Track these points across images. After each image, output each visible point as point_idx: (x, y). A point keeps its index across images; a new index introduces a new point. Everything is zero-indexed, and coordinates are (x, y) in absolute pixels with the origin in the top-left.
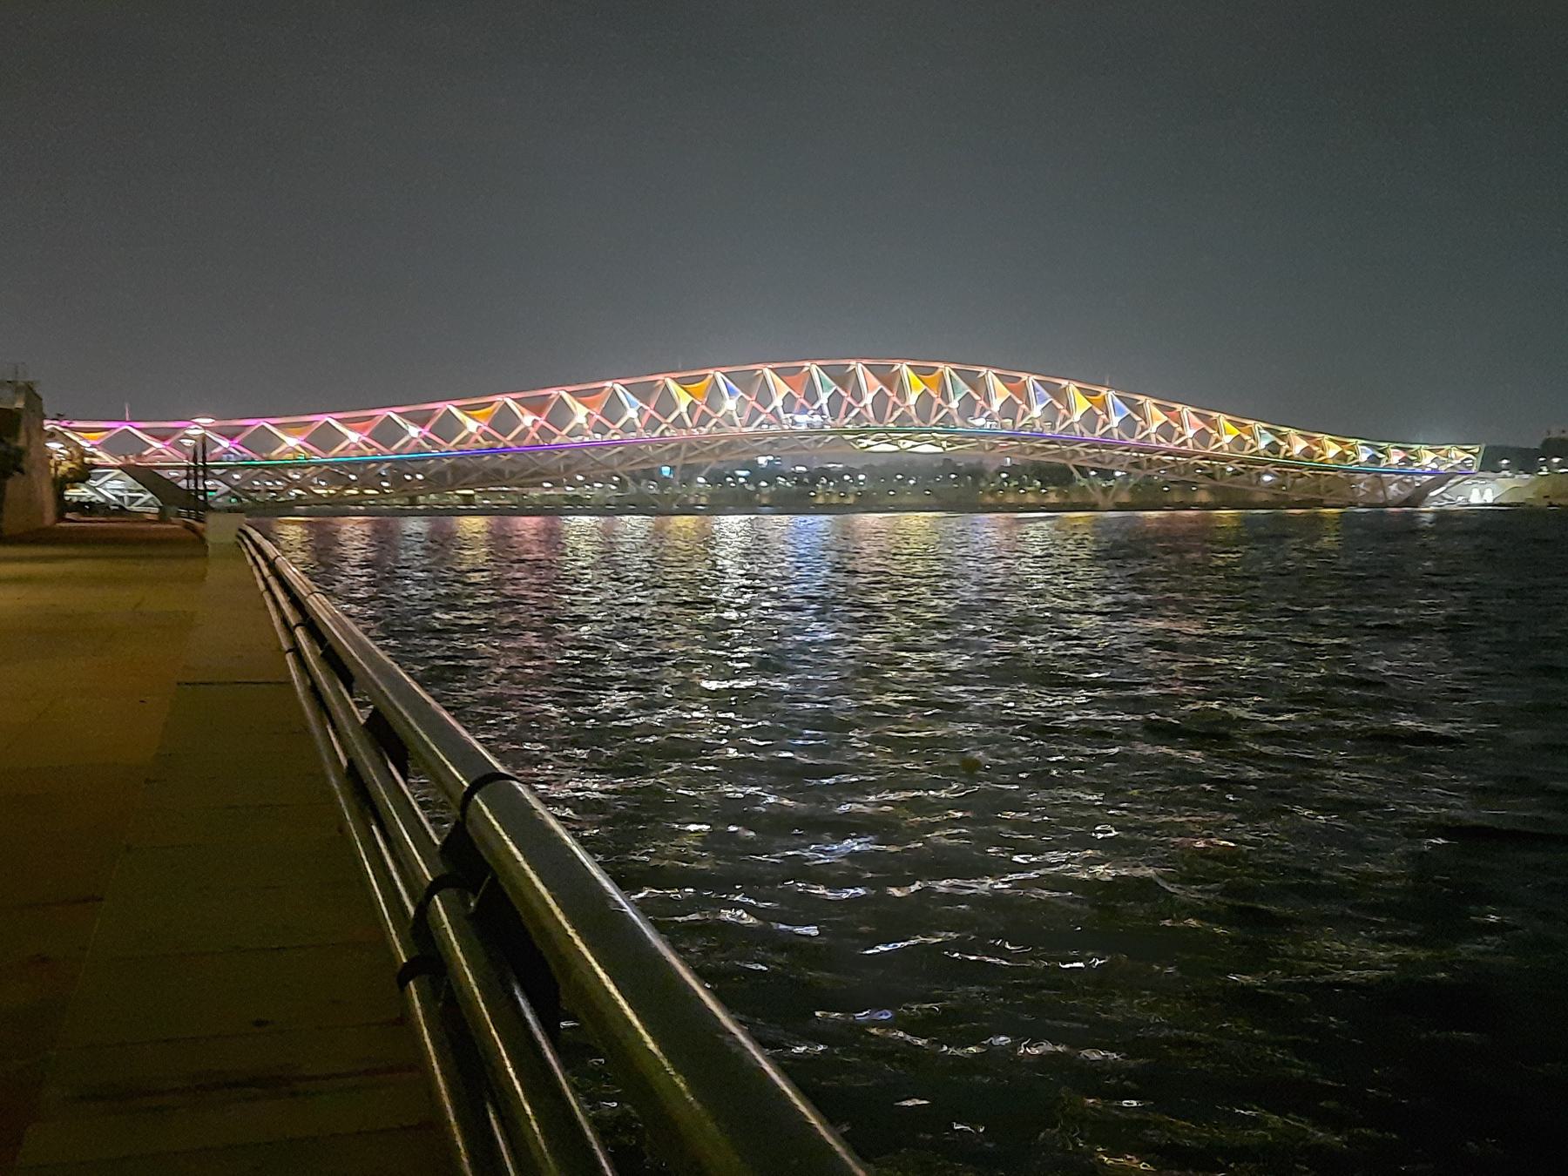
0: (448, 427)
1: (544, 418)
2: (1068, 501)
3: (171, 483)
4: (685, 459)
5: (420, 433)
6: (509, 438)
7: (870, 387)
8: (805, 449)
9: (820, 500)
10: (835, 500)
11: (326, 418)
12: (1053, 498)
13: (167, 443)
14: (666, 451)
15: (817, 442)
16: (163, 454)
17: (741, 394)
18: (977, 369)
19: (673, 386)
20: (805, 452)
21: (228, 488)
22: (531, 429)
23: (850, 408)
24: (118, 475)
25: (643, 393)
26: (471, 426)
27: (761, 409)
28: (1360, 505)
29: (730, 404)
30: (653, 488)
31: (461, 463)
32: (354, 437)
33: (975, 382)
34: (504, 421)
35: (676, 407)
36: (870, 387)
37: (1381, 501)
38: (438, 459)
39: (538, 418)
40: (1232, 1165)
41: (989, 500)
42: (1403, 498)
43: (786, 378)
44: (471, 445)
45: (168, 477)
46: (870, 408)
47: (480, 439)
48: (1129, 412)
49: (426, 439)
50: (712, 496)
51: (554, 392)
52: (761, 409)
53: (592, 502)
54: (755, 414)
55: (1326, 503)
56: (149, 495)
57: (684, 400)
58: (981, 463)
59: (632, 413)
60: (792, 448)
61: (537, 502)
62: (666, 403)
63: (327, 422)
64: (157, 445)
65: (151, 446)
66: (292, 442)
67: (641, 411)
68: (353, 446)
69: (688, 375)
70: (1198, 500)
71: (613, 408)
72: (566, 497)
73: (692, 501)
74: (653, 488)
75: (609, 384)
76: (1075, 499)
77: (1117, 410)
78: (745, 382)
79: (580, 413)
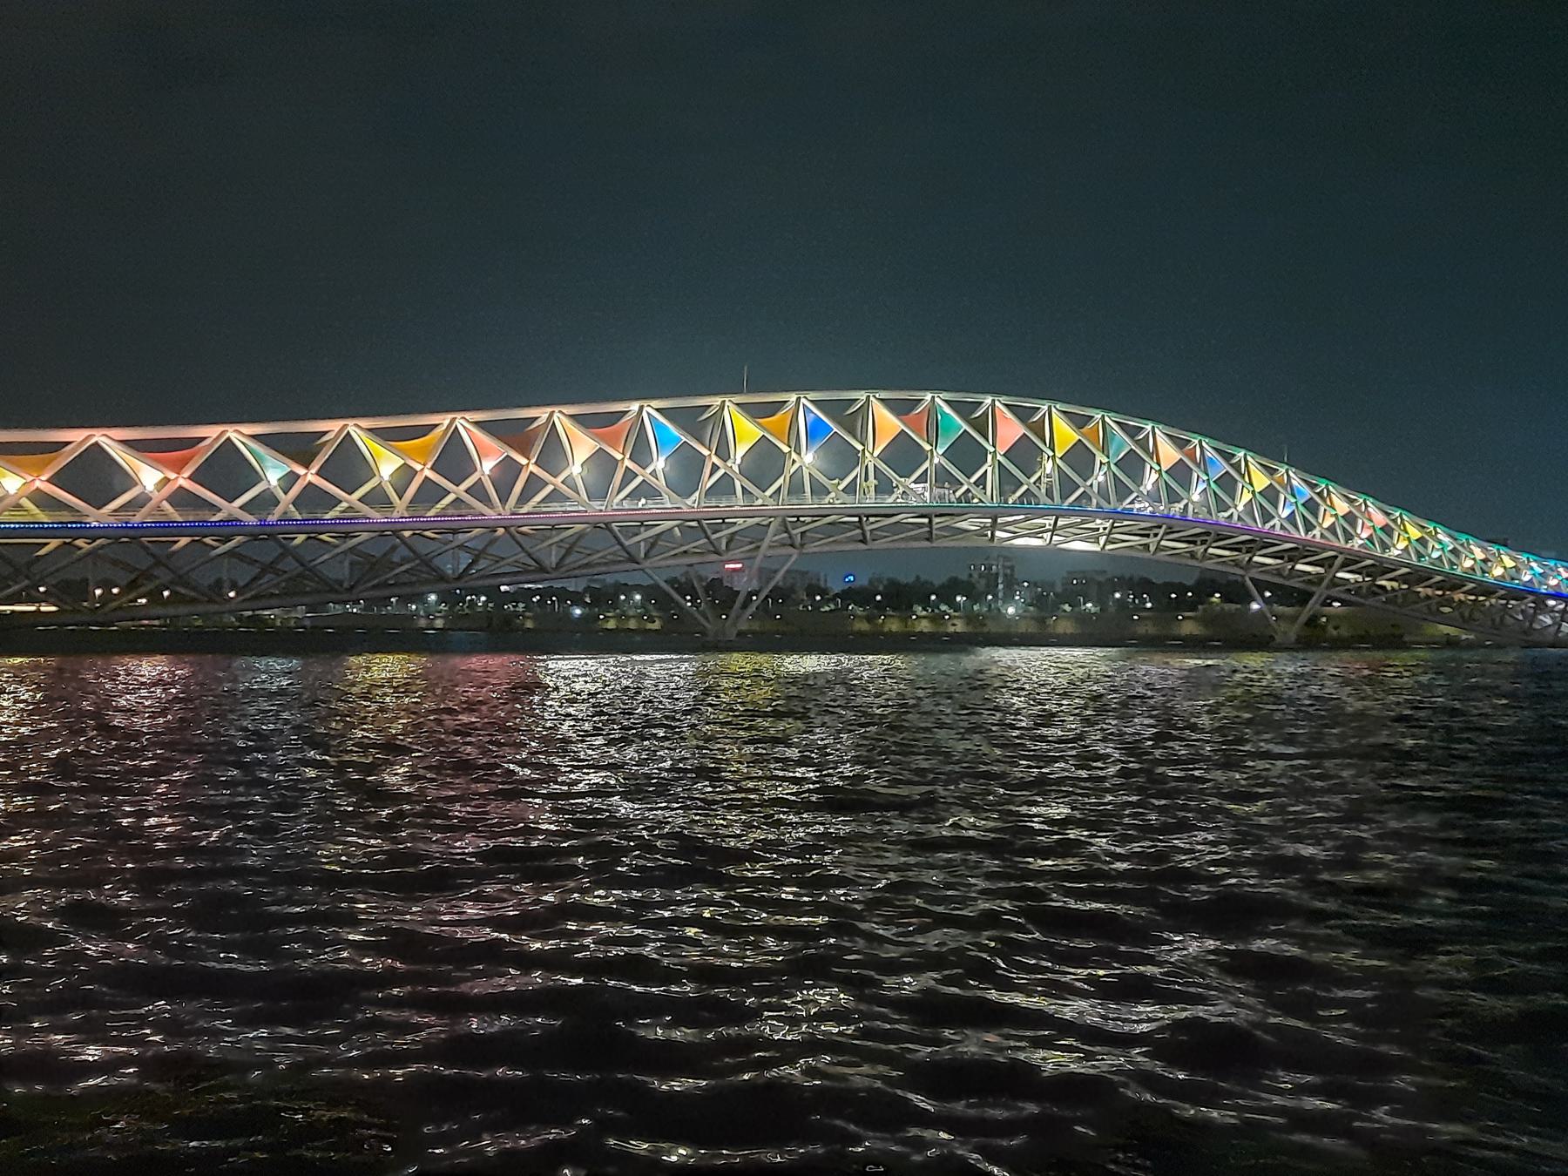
1: (315, 468)
5: (291, 478)
9: (611, 625)
32: (149, 477)
34: (454, 459)
37: (1550, 639)
39: (301, 471)
58: (918, 578)
63: (96, 444)
79: (581, 447)
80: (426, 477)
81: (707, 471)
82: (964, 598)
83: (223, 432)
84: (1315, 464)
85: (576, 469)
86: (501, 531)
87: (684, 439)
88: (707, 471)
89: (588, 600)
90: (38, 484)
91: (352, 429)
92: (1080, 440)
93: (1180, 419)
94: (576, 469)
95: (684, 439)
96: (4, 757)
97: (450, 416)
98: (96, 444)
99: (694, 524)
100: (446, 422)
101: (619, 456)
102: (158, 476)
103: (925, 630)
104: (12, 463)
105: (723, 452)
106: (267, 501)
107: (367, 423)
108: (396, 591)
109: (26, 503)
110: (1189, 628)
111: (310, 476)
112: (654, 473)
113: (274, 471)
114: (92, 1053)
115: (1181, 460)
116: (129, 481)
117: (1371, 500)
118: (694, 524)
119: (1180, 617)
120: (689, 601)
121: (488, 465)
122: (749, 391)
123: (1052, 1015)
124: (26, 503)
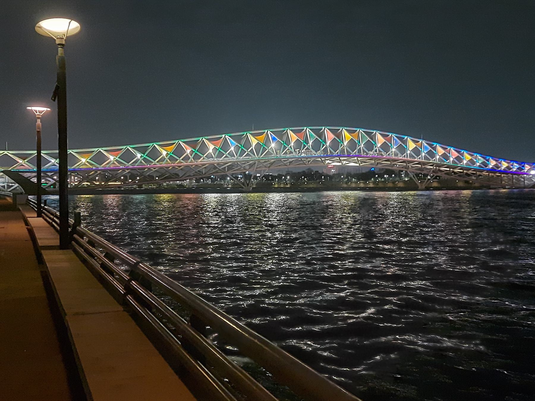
0: (155, 154)
2: (378, 186)
3: (28, 180)
4: (257, 168)
5: (142, 156)
6: (181, 158)
7: (329, 136)
8: (305, 164)
9: (276, 186)
10: (282, 186)
11: (100, 149)
12: (362, 185)
13: (25, 161)
14: (179, 170)
15: (309, 161)
16: (24, 166)
17: (278, 140)
18: (372, 131)
19: (206, 141)
20: (305, 165)
21: (54, 181)
22: (166, 157)
23: (305, 146)
24: (2, 175)
25: (238, 139)
26: (164, 153)
27: (224, 153)
28: (507, 187)
29: (273, 145)
30: (209, 182)
31: (133, 172)
32: (112, 158)
33: (320, 134)
34: (179, 151)
35: (208, 150)
36: (329, 136)
37: (523, 186)
38: (124, 170)
40: (264, 370)
41: (345, 186)
42: (531, 185)
43: (297, 134)
45: (26, 177)
46: (310, 146)
47: (168, 160)
48: (430, 148)
49: (145, 159)
50: (234, 184)
52: (224, 153)
53: (187, 187)
54: (243, 152)
55: (491, 186)
56: (17, 185)
57: (254, 142)
59: (232, 148)
60: (279, 166)
61: (166, 187)
62: (248, 144)
64: (21, 161)
65: (18, 162)
66: (83, 160)
67: (237, 148)
68: (112, 162)
69: (258, 132)
70: (433, 186)
71: (225, 146)
72: (177, 185)
73: (225, 186)
74: (209, 182)
75: (224, 136)
76: (381, 185)
77: (425, 148)
78: (280, 135)
79: (211, 147)
80: (171, 155)
81: (322, 146)
82: (387, 176)
83: (153, 145)
84: (431, 138)
85: (292, 144)
86: (236, 163)
87: (237, 144)
88: (322, 146)
89: (270, 179)
90: (117, 159)
91: (204, 139)
93: (384, 129)
94: (292, 144)
95: (316, 137)
96: (526, 268)
97: (178, 141)
98: (100, 151)
99: (300, 159)
100: (201, 139)
101: (262, 144)
102: (140, 155)
103: (401, 186)
107: (131, 146)
108: (194, 177)
109: (115, 162)
110: (371, 185)
112: (291, 147)
114: (346, 286)
115: (385, 142)
117: (453, 148)
118: (300, 159)
120: (304, 178)
121: (188, 151)
122: (254, 130)
123: (44, 189)
124: (115, 162)
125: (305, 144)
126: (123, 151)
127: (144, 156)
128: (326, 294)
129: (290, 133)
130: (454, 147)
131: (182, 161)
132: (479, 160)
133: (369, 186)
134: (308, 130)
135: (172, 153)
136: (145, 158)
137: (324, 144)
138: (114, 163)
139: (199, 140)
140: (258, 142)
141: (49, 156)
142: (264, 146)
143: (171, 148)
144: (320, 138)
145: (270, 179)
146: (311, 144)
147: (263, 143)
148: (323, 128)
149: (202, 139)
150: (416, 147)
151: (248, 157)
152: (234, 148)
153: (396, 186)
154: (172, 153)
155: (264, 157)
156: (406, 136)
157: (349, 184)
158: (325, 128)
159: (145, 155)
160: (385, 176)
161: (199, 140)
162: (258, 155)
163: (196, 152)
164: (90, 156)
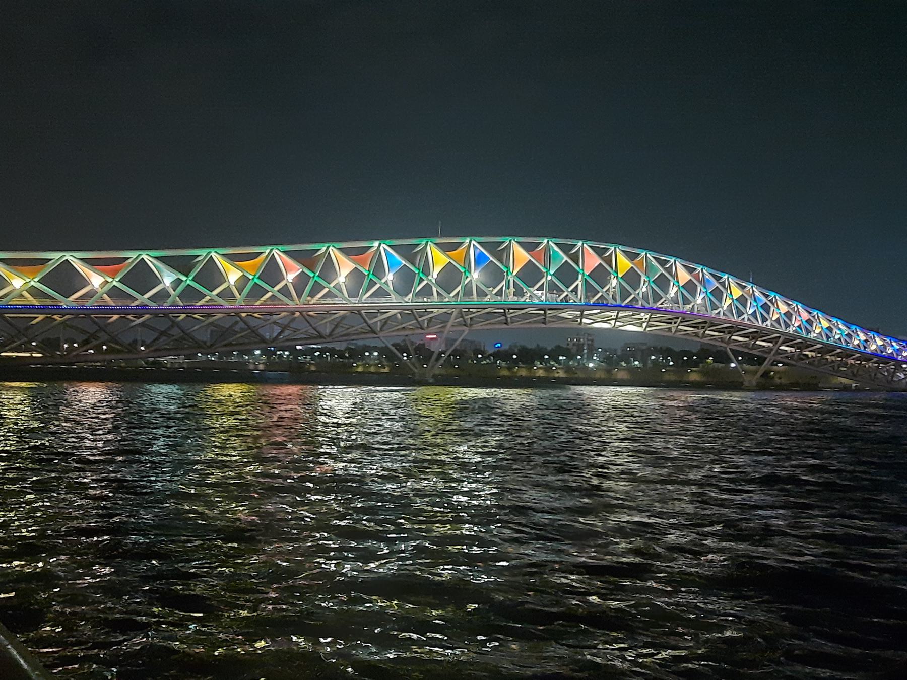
5: (178, 282)
6: (276, 288)
11: (68, 256)
32: (96, 280)
34: (272, 273)
39: (184, 278)
44: (90, 303)
51: (202, 253)
53: (169, 365)
66: (17, 283)
79: (344, 268)
92: (632, 267)
93: (691, 257)
100: (268, 251)
101: (366, 273)
103: (542, 375)
104: (17, 270)
105: (426, 271)
106: (163, 295)
110: (694, 377)
111: (188, 281)
113: (168, 278)
116: (84, 282)
117: (800, 304)
119: (355, 365)
121: (290, 277)
124: (25, 293)
125: (423, 278)
126: (54, 264)
127: (188, 282)
128: (589, 558)
129: (334, 253)
130: (802, 303)
131: (217, 298)
132: (840, 330)
133: (557, 375)
134: (382, 247)
135: (259, 278)
136: (189, 285)
137: (375, 279)
138: (22, 296)
139: (318, 250)
140: (449, 261)
141: (228, 258)
142: (371, 276)
143: (254, 266)
144: (413, 264)
145: (347, 355)
146: (435, 276)
147: (369, 271)
148: (468, 240)
149: (272, 250)
150: (742, 295)
151: (328, 300)
152: (393, 275)
153: (613, 377)
154: (257, 276)
155: (269, 303)
156: (727, 273)
157: (515, 370)
158: (470, 241)
159: (191, 278)
160: (561, 358)
161: (318, 250)
162: (299, 296)
163: (316, 278)
164: (38, 271)
